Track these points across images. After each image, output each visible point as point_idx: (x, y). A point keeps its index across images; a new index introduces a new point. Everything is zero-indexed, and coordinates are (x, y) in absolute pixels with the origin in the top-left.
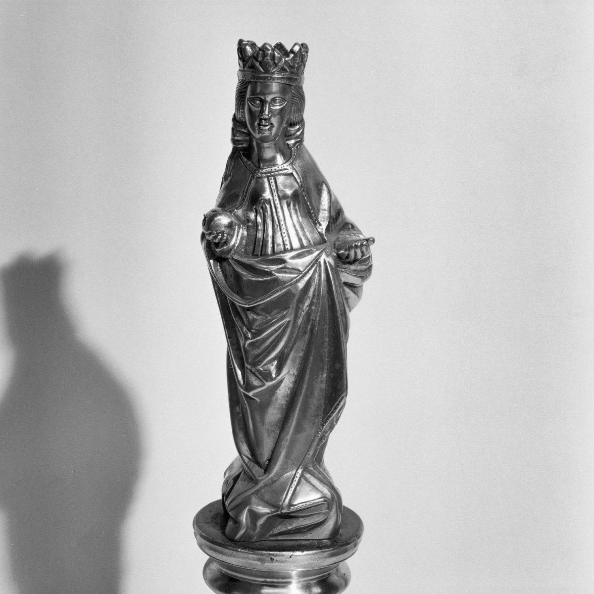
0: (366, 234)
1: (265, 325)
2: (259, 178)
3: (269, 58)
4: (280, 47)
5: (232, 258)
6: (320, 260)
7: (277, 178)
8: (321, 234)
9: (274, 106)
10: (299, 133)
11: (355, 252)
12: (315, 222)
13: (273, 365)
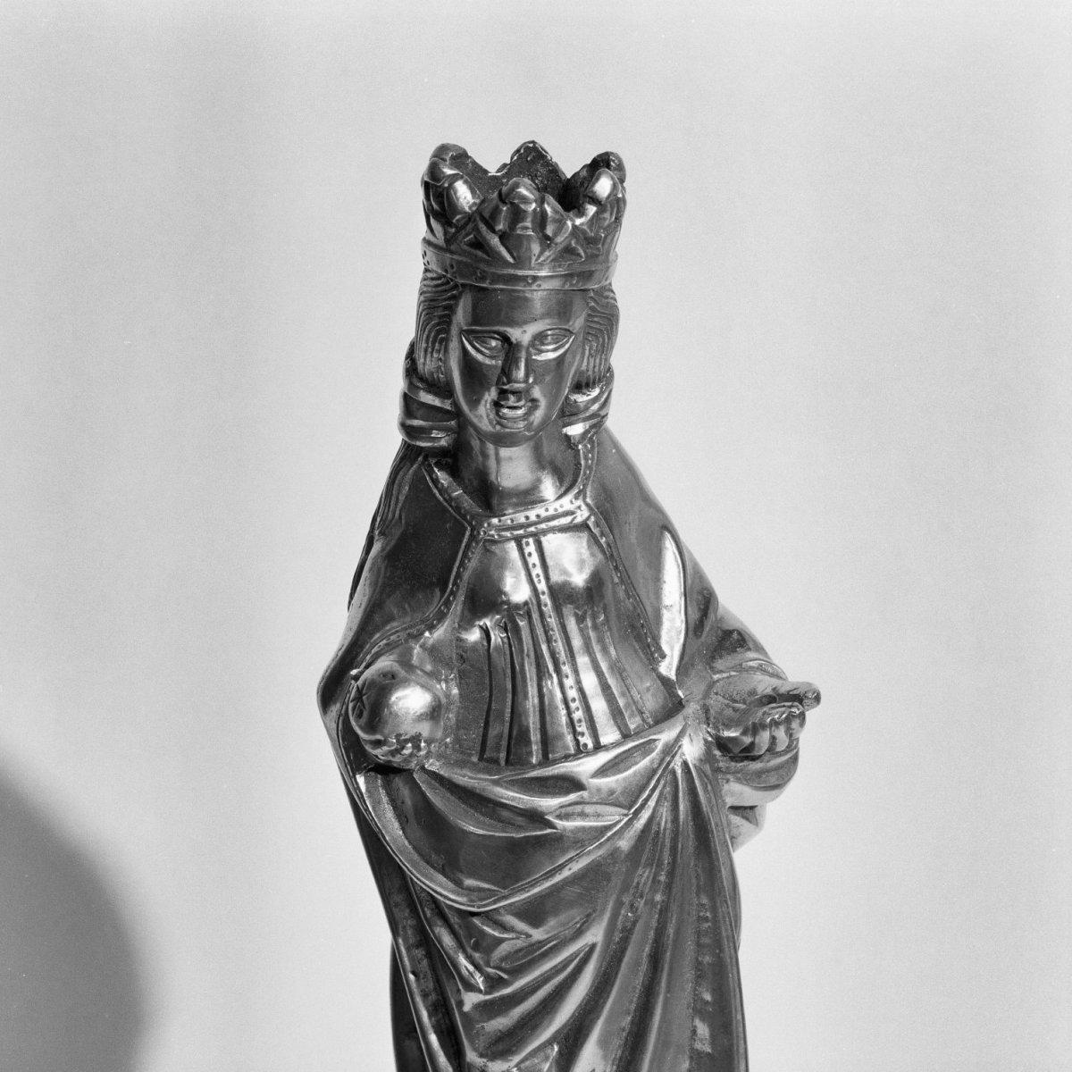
0: (796, 672)
1: (524, 957)
2: (494, 542)
3: (528, 224)
4: (531, 158)
5: (423, 768)
6: (672, 765)
7: (544, 539)
8: (665, 681)
9: (541, 352)
10: (595, 407)
11: (773, 739)
12: (650, 651)
13: (547, 1058)
